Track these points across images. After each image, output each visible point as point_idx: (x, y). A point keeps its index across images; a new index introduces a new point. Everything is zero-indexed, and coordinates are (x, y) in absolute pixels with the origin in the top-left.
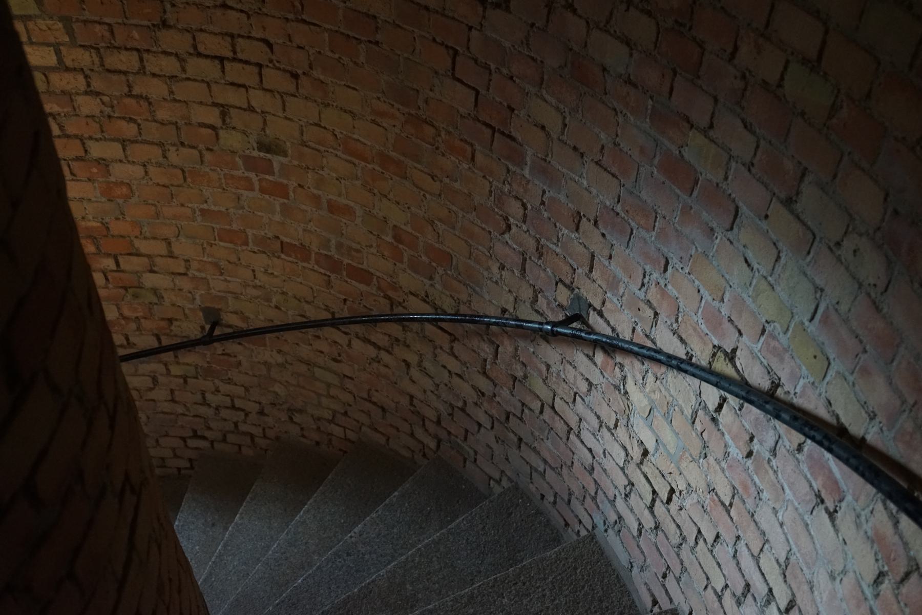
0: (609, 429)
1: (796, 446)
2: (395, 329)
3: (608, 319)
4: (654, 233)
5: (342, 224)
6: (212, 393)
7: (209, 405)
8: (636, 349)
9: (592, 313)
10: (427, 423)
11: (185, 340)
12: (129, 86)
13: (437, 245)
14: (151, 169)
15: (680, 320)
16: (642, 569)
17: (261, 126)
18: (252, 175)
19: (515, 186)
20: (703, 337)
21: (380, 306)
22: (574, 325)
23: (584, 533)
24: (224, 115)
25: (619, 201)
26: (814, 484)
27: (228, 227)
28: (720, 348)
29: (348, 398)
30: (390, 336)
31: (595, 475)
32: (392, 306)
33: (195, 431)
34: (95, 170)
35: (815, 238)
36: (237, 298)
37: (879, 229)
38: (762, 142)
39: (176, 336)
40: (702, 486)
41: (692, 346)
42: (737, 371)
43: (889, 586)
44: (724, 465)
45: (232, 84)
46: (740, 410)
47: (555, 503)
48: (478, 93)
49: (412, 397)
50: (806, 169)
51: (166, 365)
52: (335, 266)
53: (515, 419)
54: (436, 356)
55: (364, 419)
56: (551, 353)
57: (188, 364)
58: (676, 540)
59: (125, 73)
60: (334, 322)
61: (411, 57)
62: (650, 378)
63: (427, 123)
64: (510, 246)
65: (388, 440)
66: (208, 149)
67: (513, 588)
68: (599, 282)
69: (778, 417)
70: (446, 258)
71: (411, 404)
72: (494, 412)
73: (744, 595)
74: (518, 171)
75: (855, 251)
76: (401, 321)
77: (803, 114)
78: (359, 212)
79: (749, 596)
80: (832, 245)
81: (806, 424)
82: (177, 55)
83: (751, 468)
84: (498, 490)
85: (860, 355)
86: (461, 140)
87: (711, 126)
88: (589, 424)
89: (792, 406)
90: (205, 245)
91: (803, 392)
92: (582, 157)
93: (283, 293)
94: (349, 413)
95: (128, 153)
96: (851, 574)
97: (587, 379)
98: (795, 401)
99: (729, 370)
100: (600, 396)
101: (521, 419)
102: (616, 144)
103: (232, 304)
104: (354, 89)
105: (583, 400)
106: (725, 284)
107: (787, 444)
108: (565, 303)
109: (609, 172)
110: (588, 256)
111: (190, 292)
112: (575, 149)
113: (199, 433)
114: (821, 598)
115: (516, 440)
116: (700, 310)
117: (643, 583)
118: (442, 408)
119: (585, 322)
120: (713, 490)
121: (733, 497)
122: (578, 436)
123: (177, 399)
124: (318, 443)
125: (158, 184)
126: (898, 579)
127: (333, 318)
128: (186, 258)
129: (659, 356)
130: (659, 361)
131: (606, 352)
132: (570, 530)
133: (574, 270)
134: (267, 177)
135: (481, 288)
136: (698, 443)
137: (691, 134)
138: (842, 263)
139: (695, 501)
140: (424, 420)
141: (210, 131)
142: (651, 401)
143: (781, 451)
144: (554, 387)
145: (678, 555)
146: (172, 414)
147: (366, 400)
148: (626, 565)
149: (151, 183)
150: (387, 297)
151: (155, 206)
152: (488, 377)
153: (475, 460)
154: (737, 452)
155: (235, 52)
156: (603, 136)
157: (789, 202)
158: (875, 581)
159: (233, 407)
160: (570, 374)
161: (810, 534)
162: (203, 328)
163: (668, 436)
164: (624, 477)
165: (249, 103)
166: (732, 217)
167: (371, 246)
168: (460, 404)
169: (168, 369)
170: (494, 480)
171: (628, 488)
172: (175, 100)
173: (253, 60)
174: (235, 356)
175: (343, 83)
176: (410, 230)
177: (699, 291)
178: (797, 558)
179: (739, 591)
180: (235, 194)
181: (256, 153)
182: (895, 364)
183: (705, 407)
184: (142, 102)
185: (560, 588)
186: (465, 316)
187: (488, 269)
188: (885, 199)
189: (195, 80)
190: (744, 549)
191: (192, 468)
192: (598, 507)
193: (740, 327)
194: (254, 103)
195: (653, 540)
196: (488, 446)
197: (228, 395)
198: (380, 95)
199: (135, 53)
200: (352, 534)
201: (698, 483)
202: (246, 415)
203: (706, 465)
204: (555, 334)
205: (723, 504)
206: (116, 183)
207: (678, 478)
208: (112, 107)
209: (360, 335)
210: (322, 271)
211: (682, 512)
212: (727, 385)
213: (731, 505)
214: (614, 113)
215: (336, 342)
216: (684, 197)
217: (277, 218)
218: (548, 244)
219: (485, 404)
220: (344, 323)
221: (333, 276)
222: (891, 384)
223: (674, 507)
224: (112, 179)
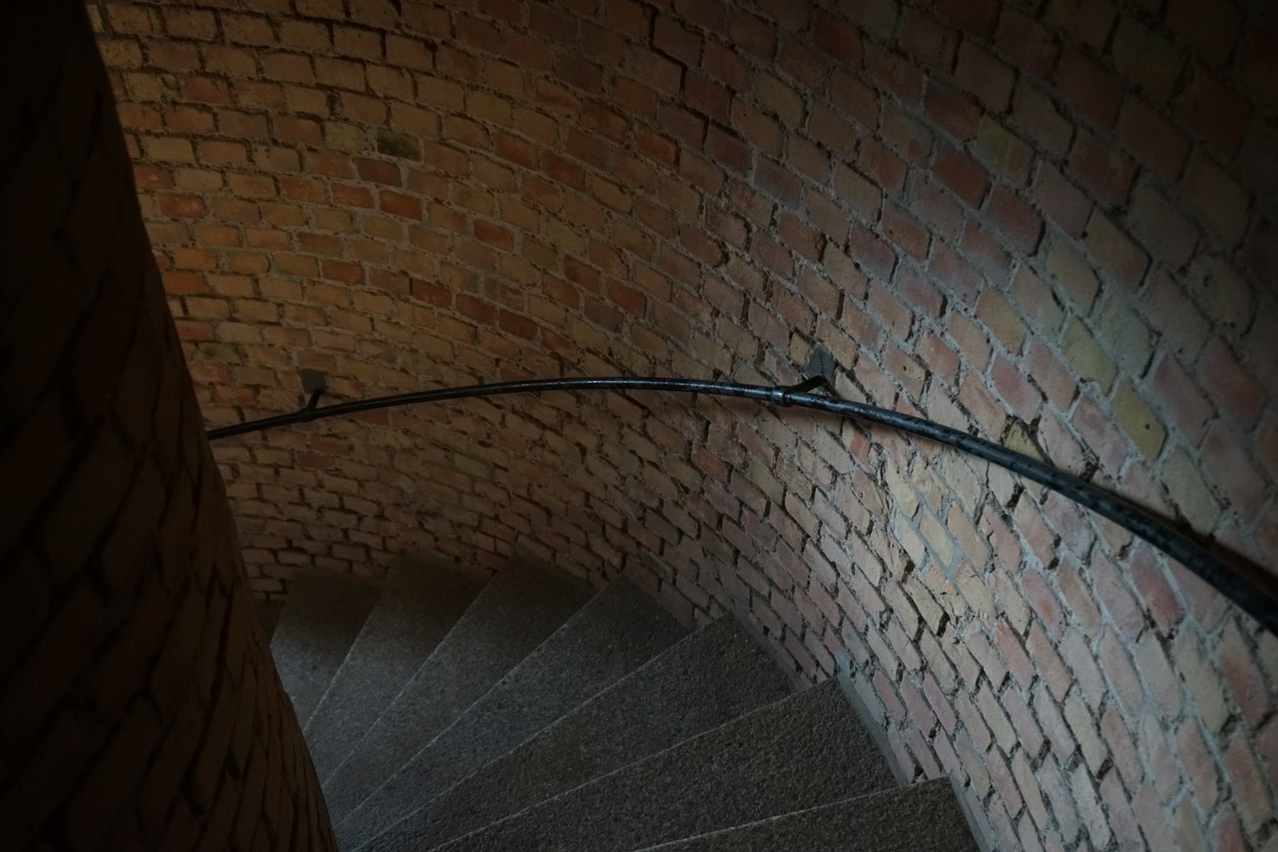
0: (860, 536)
1: (1118, 549)
2: (566, 401)
4: (928, 262)
5: (495, 255)
6: (314, 489)
7: (309, 505)
8: (900, 421)
9: (839, 374)
10: (609, 530)
11: (277, 415)
12: (202, 61)
13: (625, 283)
14: (232, 177)
15: (961, 381)
16: (902, 726)
17: (385, 117)
18: (371, 186)
19: (734, 199)
20: (992, 404)
21: (545, 368)
22: (815, 391)
23: (822, 678)
24: (332, 101)
25: (879, 218)
26: (1142, 601)
28: (1016, 418)
30: (558, 409)
31: (839, 600)
32: (562, 369)
33: (289, 542)
34: (154, 178)
35: (1150, 261)
37: (1240, 246)
39: (264, 409)
40: (987, 611)
41: (978, 417)
42: (1040, 450)
43: (1242, 734)
44: (1018, 579)
45: (344, 58)
46: (1042, 503)
47: (783, 638)
48: (685, 69)
49: (588, 495)
50: (1140, 167)
51: (250, 449)
52: (484, 313)
53: (730, 523)
54: (622, 437)
56: (781, 432)
57: (280, 449)
58: (949, 684)
59: (196, 42)
60: (481, 391)
62: (919, 463)
63: (613, 112)
64: (727, 284)
65: (554, 554)
66: (310, 149)
67: (726, 750)
68: (850, 331)
69: (1095, 507)
70: (639, 301)
71: (587, 505)
72: (701, 515)
73: (1042, 756)
74: (740, 178)
75: (1206, 279)
78: (518, 237)
79: (1049, 757)
80: (1174, 271)
82: (267, 17)
83: (1056, 583)
84: (704, 621)
85: (1210, 422)
87: (1010, 111)
89: (1112, 495)
90: (305, 284)
91: (1130, 475)
92: (829, 157)
93: (413, 351)
94: (501, 518)
95: (200, 154)
96: (1190, 721)
97: (831, 467)
98: (1118, 488)
99: (1028, 449)
100: (848, 490)
101: (738, 524)
102: (877, 139)
105: (825, 495)
106: (1025, 330)
107: (1106, 547)
108: (802, 361)
109: (866, 178)
110: (835, 295)
112: (819, 145)
114: (1148, 755)
115: (731, 553)
116: (990, 368)
117: (903, 749)
118: (628, 509)
119: (829, 387)
120: (1003, 614)
121: (1030, 624)
122: (817, 546)
123: (266, 497)
124: (458, 559)
125: (241, 198)
126: (1255, 723)
127: (481, 385)
128: (278, 301)
129: (931, 430)
132: (803, 676)
133: (816, 315)
134: (392, 188)
135: (687, 344)
136: (983, 551)
139: (978, 630)
140: (604, 527)
141: (313, 124)
142: (919, 494)
143: (1098, 556)
144: (785, 478)
145: (952, 705)
146: (257, 517)
147: (524, 498)
148: (881, 721)
149: (231, 196)
150: (555, 355)
151: (236, 227)
152: (693, 466)
153: (675, 580)
154: (1036, 562)
155: (348, 13)
156: (858, 127)
157: (1116, 214)
159: (342, 508)
160: (808, 460)
161: (1135, 669)
162: (301, 398)
163: (941, 542)
164: (879, 601)
165: (367, 84)
166: (1036, 237)
167: (534, 285)
168: (655, 504)
170: (700, 608)
171: (885, 616)
172: (265, 80)
173: (373, 24)
174: (346, 438)
175: (498, 56)
176: (588, 262)
177: (988, 341)
178: (1116, 703)
179: (1035, 751)
181: (376, 155)
182: (1258, 432)
184: (219, 83)
185: (790, 751)
186: (664, 380)
187: (696, 315)
189: (292, 52)
190: (1044, 694)
191: (285, 592)
192: (843, 642)
193: (1044, 389)
194: (374, 87)
195: (919, 686)
196: (692, 561)
197: (336, 493)
198: (549, 73)
199: (209, 13)
200: (505, 679)
202: (360, 519)
204: (788, 403)
205: (1016, 633)
207: (954, 599)
208: (178, 89)
209: (518, 408)
210: (467, 320)
211: (959, 647)
212: (1025, 467)
213: (1027, 634)
215: (484, 419)
216: (970, 209)
217: (405, 245)
218: (780, 279)
219: (689, 503)
220: (496, 392)
221: (481, 327)
223: (947, 639)
224: (178, 190)
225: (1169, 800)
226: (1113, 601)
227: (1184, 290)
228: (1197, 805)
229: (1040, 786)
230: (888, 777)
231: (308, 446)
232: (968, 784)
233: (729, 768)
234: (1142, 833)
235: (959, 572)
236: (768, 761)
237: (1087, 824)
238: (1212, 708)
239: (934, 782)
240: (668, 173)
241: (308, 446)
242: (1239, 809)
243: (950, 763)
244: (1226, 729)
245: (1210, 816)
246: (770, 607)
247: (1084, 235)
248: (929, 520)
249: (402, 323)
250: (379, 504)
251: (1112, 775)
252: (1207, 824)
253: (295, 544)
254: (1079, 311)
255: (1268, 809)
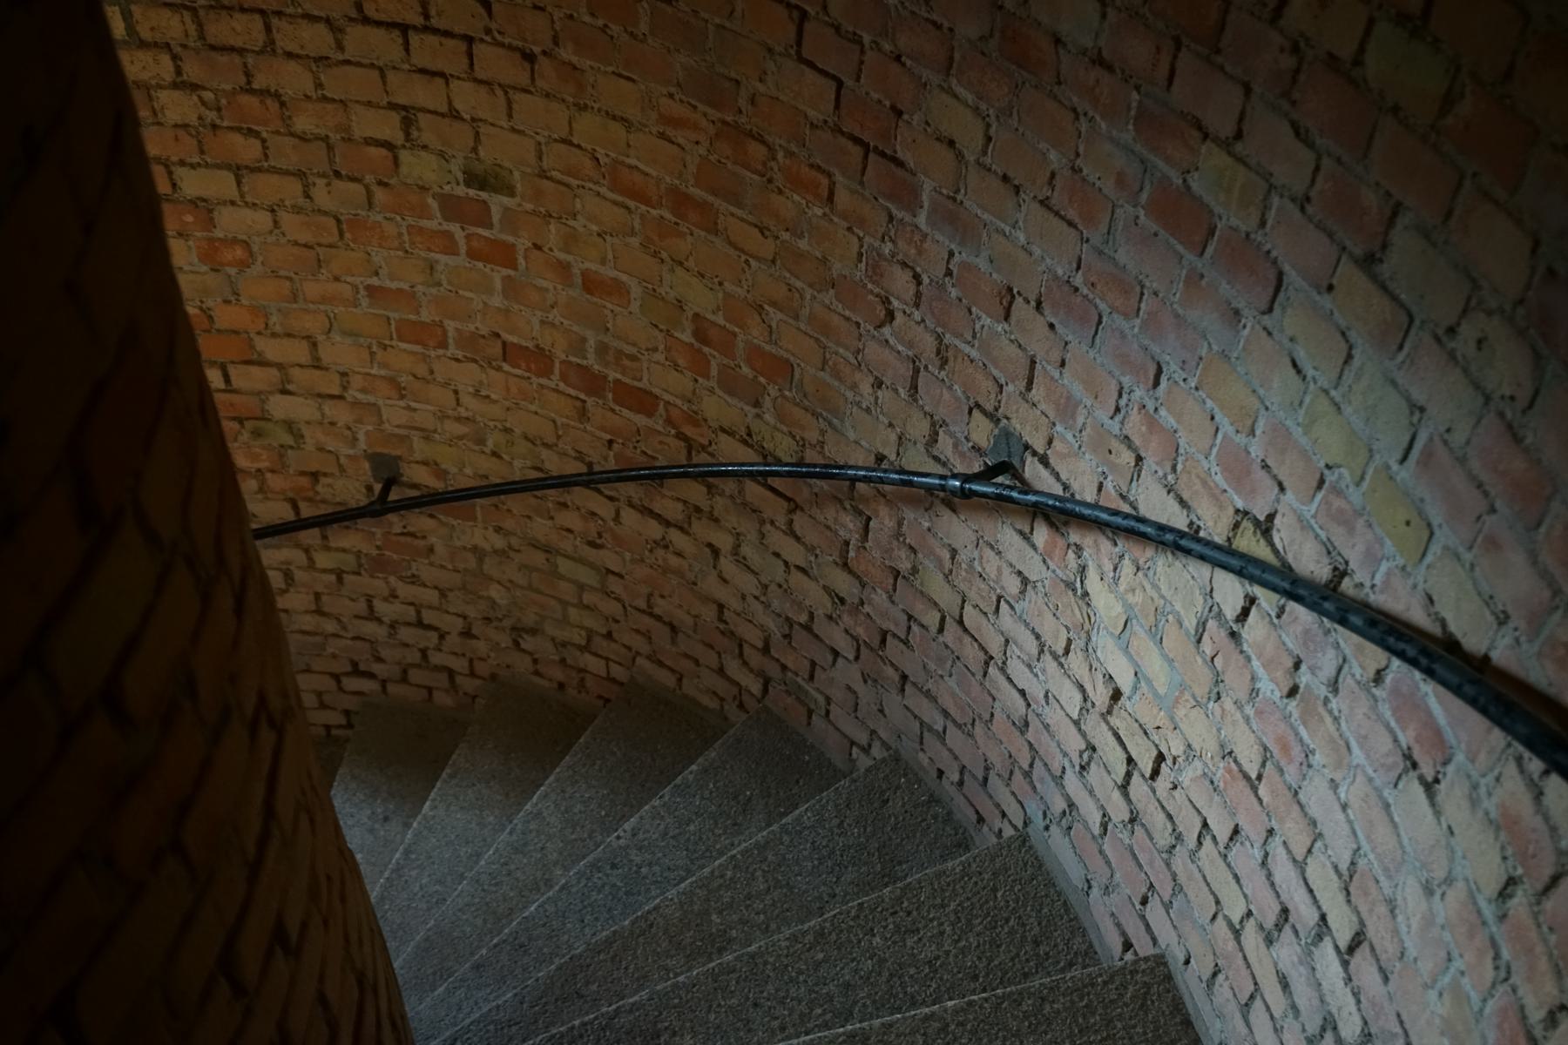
0: (1055, 657)
1: (1371, 674)
2: (695, 492)
3: (1057, 469)
4: (1138, 322)
6: (385, 600)
7: (379, 620)
8: (1104, 516)
9: (1029, 459)
10: (747, 650)
12: (248, 75)
13: (767, 348)
14: (286, 218)
15: (1179, 467)
16: (1107, 890)
17: (472, 144)
18: (454, 228)
19: (900, 243)
20: (1217, 496)
21: (670, 452)
22: (1000, 479)
23: (1008, 832)
24: (407, 124)
25: (1079, 268)
27: (413, 317)
28: (1246, 513)
29: (612, 608)
30: (685, 502)
31: (1030, 736)
32: (689, 453)
33: (355, 664)
34: (189, 218)
35: (1411, 321)
36: (427, 438)
37: (1521, 302)
38: (1326, 162)
39: (324, 501)
40: (1210, 747)
41: (1200, 512)
42: (1275, 551)
43: (1524, 900)
44: (1249, 711)
45: (423, 71)
46: (1279, 617)
47: (961, 783)
48: (840, 84)
49: (721, 607)
50: (1399, 204)
51: (307, 551)
52: (593, 384)
53: (896, 642)
54: (763, 536)
55: (638, 643)
56: (958, 529)
57: (344, 550)
58: (1164, 839)
59: (241, 51)
60: (591, 479)
61: (728, 25)
62: (1127, 567)
63: (753, 137)
64: (892, 348)
67: (890, 920)
68: (1043, 406)
69: (1343, 622)
70: (783, 369)
72: (860, 631)
73: (1279, 927)
74: (908, 218)
75: (1480, 342)
76: (707, 476)
77: (1396, 109)
78: (636, 291)
80: (1440, 332)
81: (1391, 631)
82: (328, 21)
83: (1296, 715)
84: (864, 762)
85: (1485, 517)
86: (812, 166)
87: (1239, 135)
88: (1021, 649)
89: (1364, 607)
90: (374, 349)
92: (1017, 193)
93: (507, 431)
94: (615, 635)
95: (246, 189)
96: (1460, 884)
97: (1020, 573)
99: (1261, 551)
100: (1040, 601)
101: (906, 642)
102: (1076, 170)
103: (420, 448)
104: (629, 79)
105: (1012, 607)
106: (1257, 404)
107: (1358, 671)
108: (984, 444)
109: (1063, 218)
111: (349, 428)
112: (1005, 178)
113: (362, 667)
114: (1409, 927)
115: (897, 678)
116: (1215, 451)
117: (1108, 920)
118: (771, 624)
119: (1017, 475)
120: (1230, 753)
121: (1263, 765)
122: (1003, 670)
123: (326, 609)
124: (561, 686)
125: (296, 243)
126: (1539, 887)
127: (591, 473)
128: (342, 369)
130: (1143, 535)
131: (1051, 524)
132: (985, 829)
134: (480, 231)
135: (842, 421)
136: (1206, 676)
137: (1204, 149)
138: (1457, 363)
139: (1199, 772)
140: (741, 646)
141: (384, 152)
142: (1128, 607)
143: (1346, 683)
144: (962, 586)
145: (1168, 865)
146: (316, 634)
147: (643, 612)
148: (1081, 884)
149: (283, 240)
150: (680, 436)
152: (851, 572)
153: (828, 712)
154: (1271, 689)
155: (427, 16)
156: (1053, 155)
157: (1368, 262)
158: (1501, 894)
159: (420, 624)
160: (991, 564)
161: (1392, 820)
162: (369, 488)
163: (1154, 665)
164: (1079, 737)
165: (450, 103)
166: (1271, 290)
167: (655, 350)
168: (803, 618)
169: (310, 559)
170: (859, 746)
171: (1085, 756)
172: (325, 99)
173: (456, 30)
174: (424, 537)
175: (610, 69)
176: (722, 322)
177: (1213, 418)
179: (1270, 921)
180: (425, 259)
181: (461, 190)
182: (1543, 529)
183: (1220, 614)
184: (269, 102)
185: (969, 921)
186: (815, 466)
187: (854, 387)
188: (1534, 251)
190: (1281, 851)
192: (1034, 788)
193: (1281, 477)
194: (458, 105)
195: (1127, 841)
196: (849, 688)
197: (412, 604)
198: (673, 90)
199: (257, 17)
200: (620, 832)
201: (1204, 740)
202: (442, 637)
203: (1218, 712)
204: (966, 495)
205: (1246, 777)
206: (223, 241)
207: (1170, 735)
208: (219, 109)
209: (636, 501)
210: (573, 392)
211: (1176, 793)
212: (1257, 572)
213: (1259, 777)
214: (1073, 115)
215: (594, 514)
216: (1190, 257)
217: (497, 301)
218: (957, 342)
219: (846, 617)
220: (609, 481)
221: (590, 401)
222: (1535, 563)
223: (1162, 784)
224: (218, 233)
225: (1435, 981)
226: (1365, 737)
227: (1452, 355)
228: (1468, 987)
229: (1276, 965)
230: (1090, 954)
231: (378, 547)
232: (1187, 962)
233: (895, 943)
234: (1401, 1022)
235: (1177, 701)
236: (942, 933)
237: (1334, 1011)
238: (1488, 870)
239: (1146, 959)
240: (819, 212)
241: (378, 547)
242: (1521, 992)
243: (1166, 936)
244: (1504, 894)
245: (1485, 1000)
246: (945, 745)
247: (1330, 288)
248: (1141, 639)
249: (493, 396)
250: (465, 618)
251: (1364, 950)
252: (1481, 1010)
253: (362, 667)
254: (1323, 382)
255: (1555, 992)
